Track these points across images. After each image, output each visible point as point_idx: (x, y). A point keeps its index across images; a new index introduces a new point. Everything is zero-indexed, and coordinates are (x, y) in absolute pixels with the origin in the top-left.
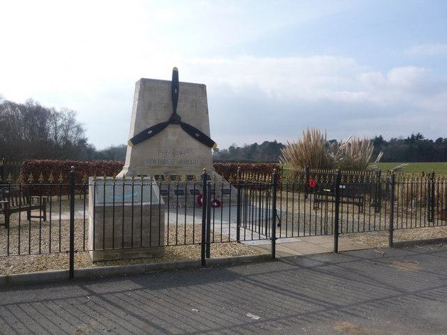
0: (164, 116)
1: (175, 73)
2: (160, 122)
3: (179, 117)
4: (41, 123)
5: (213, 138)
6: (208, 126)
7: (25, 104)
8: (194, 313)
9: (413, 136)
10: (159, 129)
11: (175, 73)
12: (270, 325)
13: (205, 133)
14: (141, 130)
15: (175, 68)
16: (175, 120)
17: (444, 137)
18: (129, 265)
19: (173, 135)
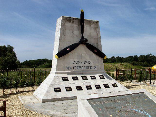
0: (77, 40)
1: (82, 14)
2: (74, 43)
3: (86, 40)
4: (13, 85)
5: (104, 52)
6: (101, 48)
7: (68, 22)
8: (111, 115)
9: (148, 54)
10: (73, 47)
11: (82, 14)
12: (22, 79)
13: (99, 49)
14: (63, 48)
15: (82, 10)
16: (83, 41)
17: (154, 54)
18: (43, 110)
19: (82, 50)
